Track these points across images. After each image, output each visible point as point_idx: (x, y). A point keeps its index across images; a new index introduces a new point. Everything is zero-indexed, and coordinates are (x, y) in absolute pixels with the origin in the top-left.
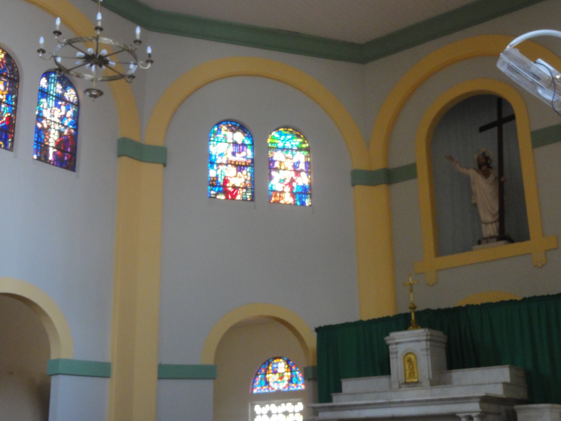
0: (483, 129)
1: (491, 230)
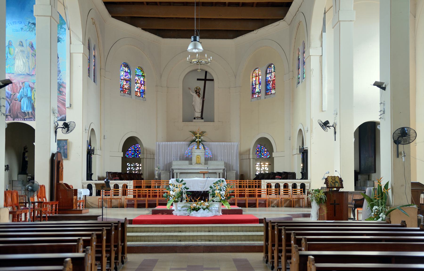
0: (198, 80)
1: (198, 115)
